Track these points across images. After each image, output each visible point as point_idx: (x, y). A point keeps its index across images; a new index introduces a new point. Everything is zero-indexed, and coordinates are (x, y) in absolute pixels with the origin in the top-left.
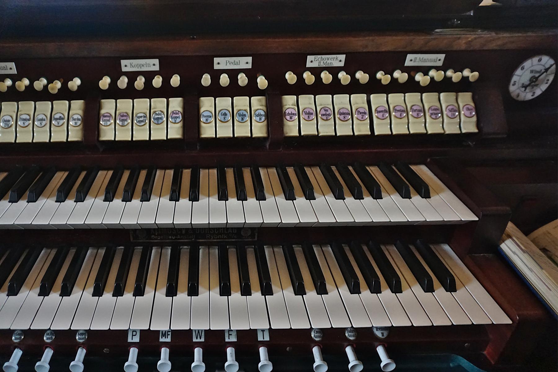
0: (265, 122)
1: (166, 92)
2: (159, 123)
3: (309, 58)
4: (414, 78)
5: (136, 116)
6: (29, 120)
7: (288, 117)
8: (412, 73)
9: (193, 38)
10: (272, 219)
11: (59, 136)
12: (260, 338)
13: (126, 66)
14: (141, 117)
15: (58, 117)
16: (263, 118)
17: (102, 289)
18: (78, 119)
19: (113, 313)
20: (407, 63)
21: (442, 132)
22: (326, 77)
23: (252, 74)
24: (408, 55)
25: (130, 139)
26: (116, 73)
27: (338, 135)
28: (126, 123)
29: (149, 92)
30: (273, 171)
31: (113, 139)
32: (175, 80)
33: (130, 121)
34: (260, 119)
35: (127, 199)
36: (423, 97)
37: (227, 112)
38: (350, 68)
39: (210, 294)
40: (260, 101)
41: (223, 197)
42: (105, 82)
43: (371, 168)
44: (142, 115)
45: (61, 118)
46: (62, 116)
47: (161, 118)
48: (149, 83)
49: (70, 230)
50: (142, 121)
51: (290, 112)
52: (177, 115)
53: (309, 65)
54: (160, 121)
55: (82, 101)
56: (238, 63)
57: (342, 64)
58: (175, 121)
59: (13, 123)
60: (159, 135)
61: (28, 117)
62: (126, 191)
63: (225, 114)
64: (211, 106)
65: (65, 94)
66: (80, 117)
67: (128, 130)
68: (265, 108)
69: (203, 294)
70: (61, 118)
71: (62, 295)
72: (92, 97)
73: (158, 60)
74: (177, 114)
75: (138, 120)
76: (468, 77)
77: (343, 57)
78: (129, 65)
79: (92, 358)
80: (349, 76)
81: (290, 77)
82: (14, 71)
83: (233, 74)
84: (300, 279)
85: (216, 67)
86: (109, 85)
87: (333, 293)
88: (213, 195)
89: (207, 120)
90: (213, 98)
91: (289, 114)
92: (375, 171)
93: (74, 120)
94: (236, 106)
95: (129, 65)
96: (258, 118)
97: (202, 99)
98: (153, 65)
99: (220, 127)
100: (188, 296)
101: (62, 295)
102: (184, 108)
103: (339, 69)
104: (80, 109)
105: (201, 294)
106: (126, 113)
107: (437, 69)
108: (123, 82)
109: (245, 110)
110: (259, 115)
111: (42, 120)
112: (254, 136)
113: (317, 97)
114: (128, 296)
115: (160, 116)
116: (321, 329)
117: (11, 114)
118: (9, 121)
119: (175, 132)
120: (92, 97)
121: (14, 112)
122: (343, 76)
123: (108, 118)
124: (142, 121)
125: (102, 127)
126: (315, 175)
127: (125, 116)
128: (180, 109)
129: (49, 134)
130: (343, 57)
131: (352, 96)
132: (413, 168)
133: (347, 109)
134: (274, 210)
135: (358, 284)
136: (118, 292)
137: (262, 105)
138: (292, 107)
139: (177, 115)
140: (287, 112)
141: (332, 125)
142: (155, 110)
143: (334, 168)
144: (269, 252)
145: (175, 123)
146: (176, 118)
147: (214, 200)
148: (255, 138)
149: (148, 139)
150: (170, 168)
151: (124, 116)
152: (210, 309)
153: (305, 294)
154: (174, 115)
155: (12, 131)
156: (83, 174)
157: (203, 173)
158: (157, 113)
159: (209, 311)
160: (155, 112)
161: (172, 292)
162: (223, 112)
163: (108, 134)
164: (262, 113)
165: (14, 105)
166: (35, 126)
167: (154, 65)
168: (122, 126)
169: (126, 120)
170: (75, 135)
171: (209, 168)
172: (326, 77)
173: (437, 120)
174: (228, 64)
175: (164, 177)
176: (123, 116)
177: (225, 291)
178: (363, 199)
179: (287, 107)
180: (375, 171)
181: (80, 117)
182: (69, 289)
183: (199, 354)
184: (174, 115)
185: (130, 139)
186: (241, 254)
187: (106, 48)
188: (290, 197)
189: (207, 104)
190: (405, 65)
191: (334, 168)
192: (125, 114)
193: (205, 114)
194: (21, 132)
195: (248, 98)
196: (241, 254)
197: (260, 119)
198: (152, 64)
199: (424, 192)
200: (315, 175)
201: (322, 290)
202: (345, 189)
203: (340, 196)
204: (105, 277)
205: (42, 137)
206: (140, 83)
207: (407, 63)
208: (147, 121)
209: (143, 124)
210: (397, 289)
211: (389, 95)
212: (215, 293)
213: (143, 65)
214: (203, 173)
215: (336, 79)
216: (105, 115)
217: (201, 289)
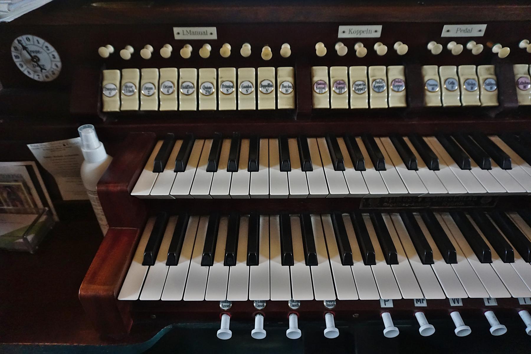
0: (496, 92)
1: (391, 59)
2: (380, 91)
3: (341, 28)
4: (491, 49)
5: (354, 83)
6: (233, 87)
7: (521, 87)
8: (489, 44)
9: (421, 4)
10: (320, 191)
11: (267, 104)
12: (383, 305)
13: (178, 33)
14: (360, 85)
15: (267, 84)
16: (291, 90)
17: (176, 258)
18: (289, 87)
19: (249, 283)
20: (444, 34)
21: (480, 104)
22: (360, 50)
23: (216, 45)
24: (445, 26)
25: (235, 109)
26: (331, 42)
27: (332, 107)
28: (343, 91)
29: (372, 59)
30: (323, 142)
31: (176, 109)
32: (286, 49)
33: (346, 89)
34: (491, 88)
35: (233, 168)
36: (459, 70)
37: (454, 81)
38: (387, 38)
39: (270, 263)
40: (488, 69)
41: (285, 167)
42: (107, 51)
43: (383, 139)
44: (361, 83)
45: (269, 86)
46: (271, 83)
47: (383, 87)
48: (195, 52)
49: (157, 199)
50: (362, 89)
51: (524, 81)
52: (400, 84)
53: (340, 35)
54: (381, 90)
55: (291, 68)
56: (205, 33)
57: (378, 35)
58: (398, 89)
59: (214, 90)
60: (379, 102)
61: (232, 84)
62: (178, 159)
63: (453, 83)
64: (435, 75)
65: (277, 61)
66: (290, 85)
67: (345, 98)
68: (494, 77)
69: (264, 263)
70: (269, 86)
71: (169, 264)
72: (303, 64)
73: (215, 28)
74: (399, 82)
75: (357, 88)
76: (526, 48)
77: (379, 28)
78: (181, 32)
79: (180, 324)
80: (386, 47)
81: (434, 47)
82: (215, 37)
83: (197, 45)
84: (372, 249)
85: (177, 37)
86: (172, 53)
87: (403, 263)
88: (275, 165)
89: (433, 89)
90: (215, 70)
91: (522, 83)
92: (432, 142)
93: (285, 87)
94: (221, 78)
95: (347, 32)
96: (488, 88)
97: (425, 67)
98: (374, 31)
99: (354, 98)
100: (167, 265)
101: (169, 264)
102: (405, 74)
103: (375, 40)
104: (289, 76)
105: (182, 262)
106: (342, 80)
107: (478, 40)
108: (167, 51)
109: (474, 79)
110: (489, 84)
111: (248, 87)
112: (332, 107)
113: (239, 69)
114: (241, 266)
115: (381, 85)
116: (497, 299)
117: (211, 81)
118: (210, 88)
119: (397, 100)
120: (303, 64)
121: (214, 78)
122: (381, 49)
123: (323, 86)
124: (362, 89)
125: (105, 99)
126: (385, 144)
127: (342, 84)
128: (402, 78)
129: (138, 102)
130: (379, 28)
131: (370, 68)
132: (425, 139)
133: (436, 81)
134: (395, 180)
135: (490, 253)
136: (230, 261)
137: (491, 74)
138: (525, 76)
139: (400, 84)
140: (520, 81)
141: (175, 99)
142: (375, 78)
143: (406, 139)
144: (316, 221)
145: (398, 91)
146: (399, 86)
147: (275, 170)
148: (333, 109)
149: (195, 109)
150: (209, 138)
151: (340, 84)
152: (333, 279)
153: (433, 263)
154: (397, 84)
155: (213, 99)
156: (159, 145)
157: (263, 143)
158: (378, 81)
159: (270, 281)
160: (374, 80)
161: (207, 261)
162: (451, 80)
163: (322, 102)
164: (493, 82)
165: (214, 72)
166: (141, 95)
167: (211, 34)
168: (339, 94)
169: (343, 88)
170: (286, 102)
171: (269, 137)
172: (360, 50)
173: (341, 95)
174: (459, 32)
175: (202, 148)
176: (340, 84)
177: (288, 260)
178: (491, 169)
179: (519, 76)
180: (432, 142)
181: (290, 85)
182: (176, 258)
183: (294, 322)
184: (397, 84)
185: (235, 109)
186: (361, 225)
187: (324, 14)
188: (339, 166)
189: (320, 73)
190: (442, 36)
191: (406, 139)
192: (341, 82)
193: (431, 82)
194: (223, 99)
195: (235, 69)
196: (361, 225)
197: (491, 88)
198: (209, 33)
199: (433, 164)
200: (385, 144)
201: (392, 260)
202: (419, 159)
203: (412, 166)
204: (179, 246)
205: (247, 104)
206: (187, 52)
207: (444, 34)
208: (366, 90)
209: (362, 92)
210: (451, 259)
211: (351, 68)
212: (277, 262)
213: (363, 32)
214: (263, 143)
215: (371, 51)
216: (319, 82)
217: (261, 258)
